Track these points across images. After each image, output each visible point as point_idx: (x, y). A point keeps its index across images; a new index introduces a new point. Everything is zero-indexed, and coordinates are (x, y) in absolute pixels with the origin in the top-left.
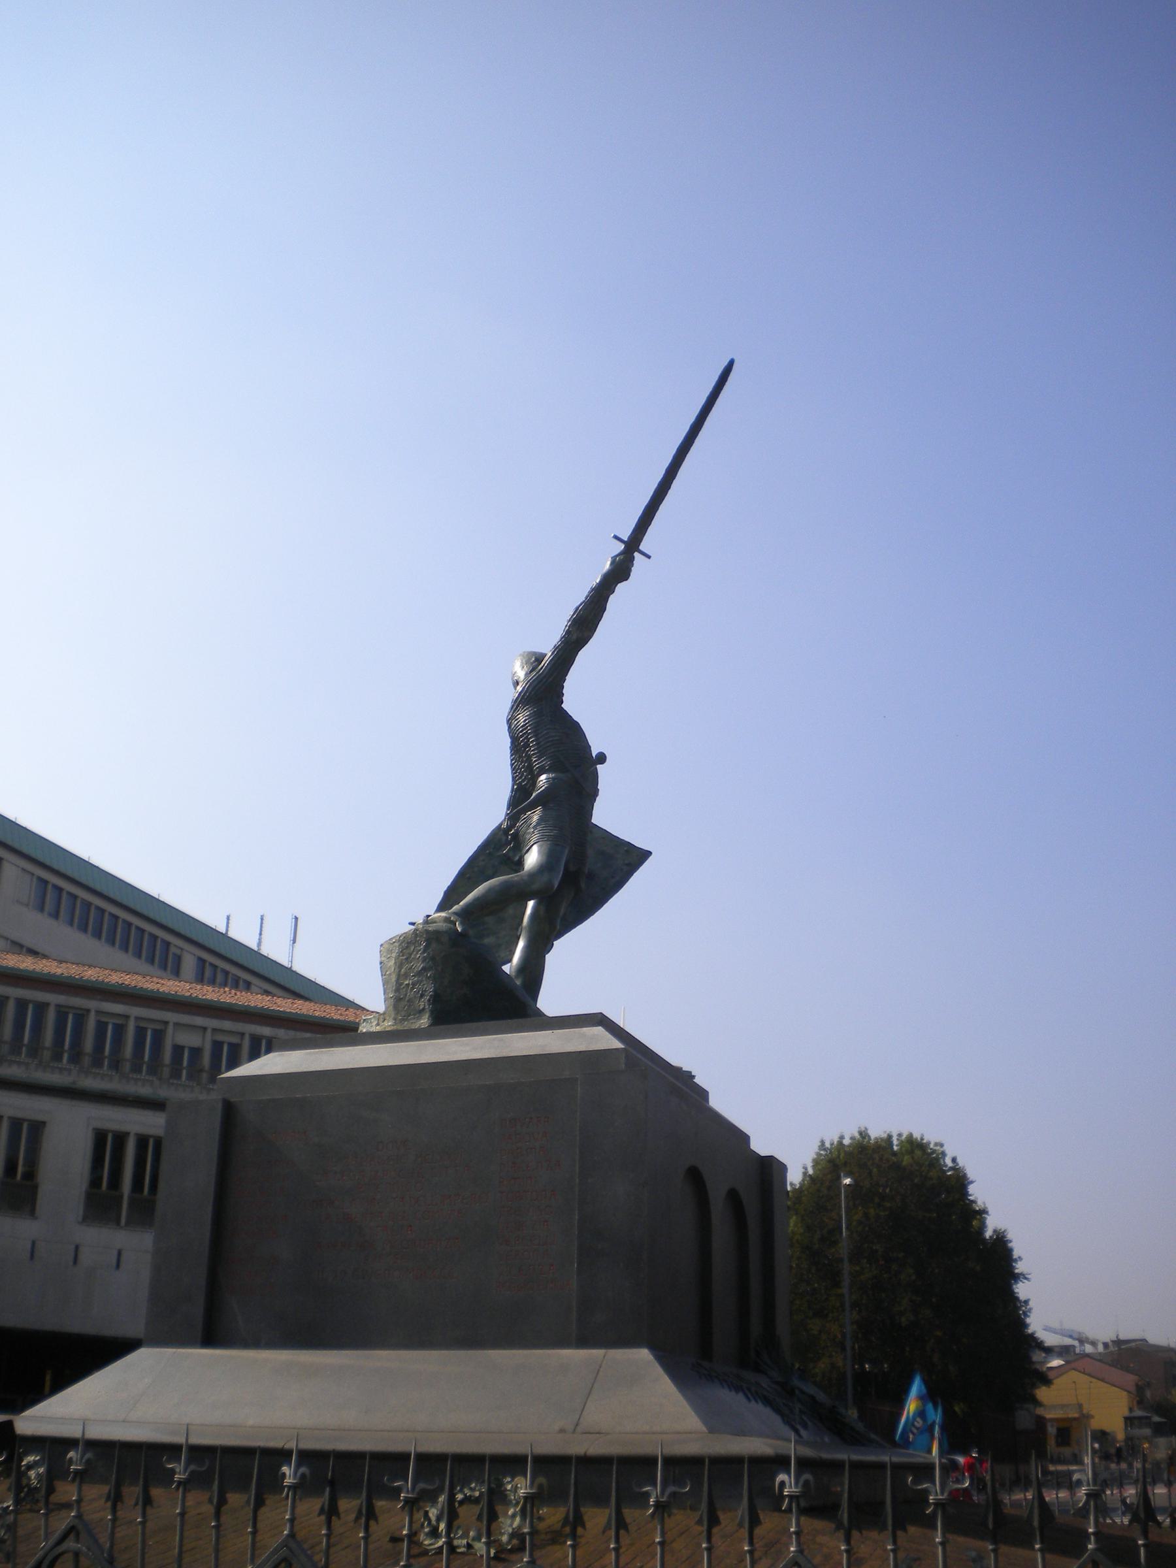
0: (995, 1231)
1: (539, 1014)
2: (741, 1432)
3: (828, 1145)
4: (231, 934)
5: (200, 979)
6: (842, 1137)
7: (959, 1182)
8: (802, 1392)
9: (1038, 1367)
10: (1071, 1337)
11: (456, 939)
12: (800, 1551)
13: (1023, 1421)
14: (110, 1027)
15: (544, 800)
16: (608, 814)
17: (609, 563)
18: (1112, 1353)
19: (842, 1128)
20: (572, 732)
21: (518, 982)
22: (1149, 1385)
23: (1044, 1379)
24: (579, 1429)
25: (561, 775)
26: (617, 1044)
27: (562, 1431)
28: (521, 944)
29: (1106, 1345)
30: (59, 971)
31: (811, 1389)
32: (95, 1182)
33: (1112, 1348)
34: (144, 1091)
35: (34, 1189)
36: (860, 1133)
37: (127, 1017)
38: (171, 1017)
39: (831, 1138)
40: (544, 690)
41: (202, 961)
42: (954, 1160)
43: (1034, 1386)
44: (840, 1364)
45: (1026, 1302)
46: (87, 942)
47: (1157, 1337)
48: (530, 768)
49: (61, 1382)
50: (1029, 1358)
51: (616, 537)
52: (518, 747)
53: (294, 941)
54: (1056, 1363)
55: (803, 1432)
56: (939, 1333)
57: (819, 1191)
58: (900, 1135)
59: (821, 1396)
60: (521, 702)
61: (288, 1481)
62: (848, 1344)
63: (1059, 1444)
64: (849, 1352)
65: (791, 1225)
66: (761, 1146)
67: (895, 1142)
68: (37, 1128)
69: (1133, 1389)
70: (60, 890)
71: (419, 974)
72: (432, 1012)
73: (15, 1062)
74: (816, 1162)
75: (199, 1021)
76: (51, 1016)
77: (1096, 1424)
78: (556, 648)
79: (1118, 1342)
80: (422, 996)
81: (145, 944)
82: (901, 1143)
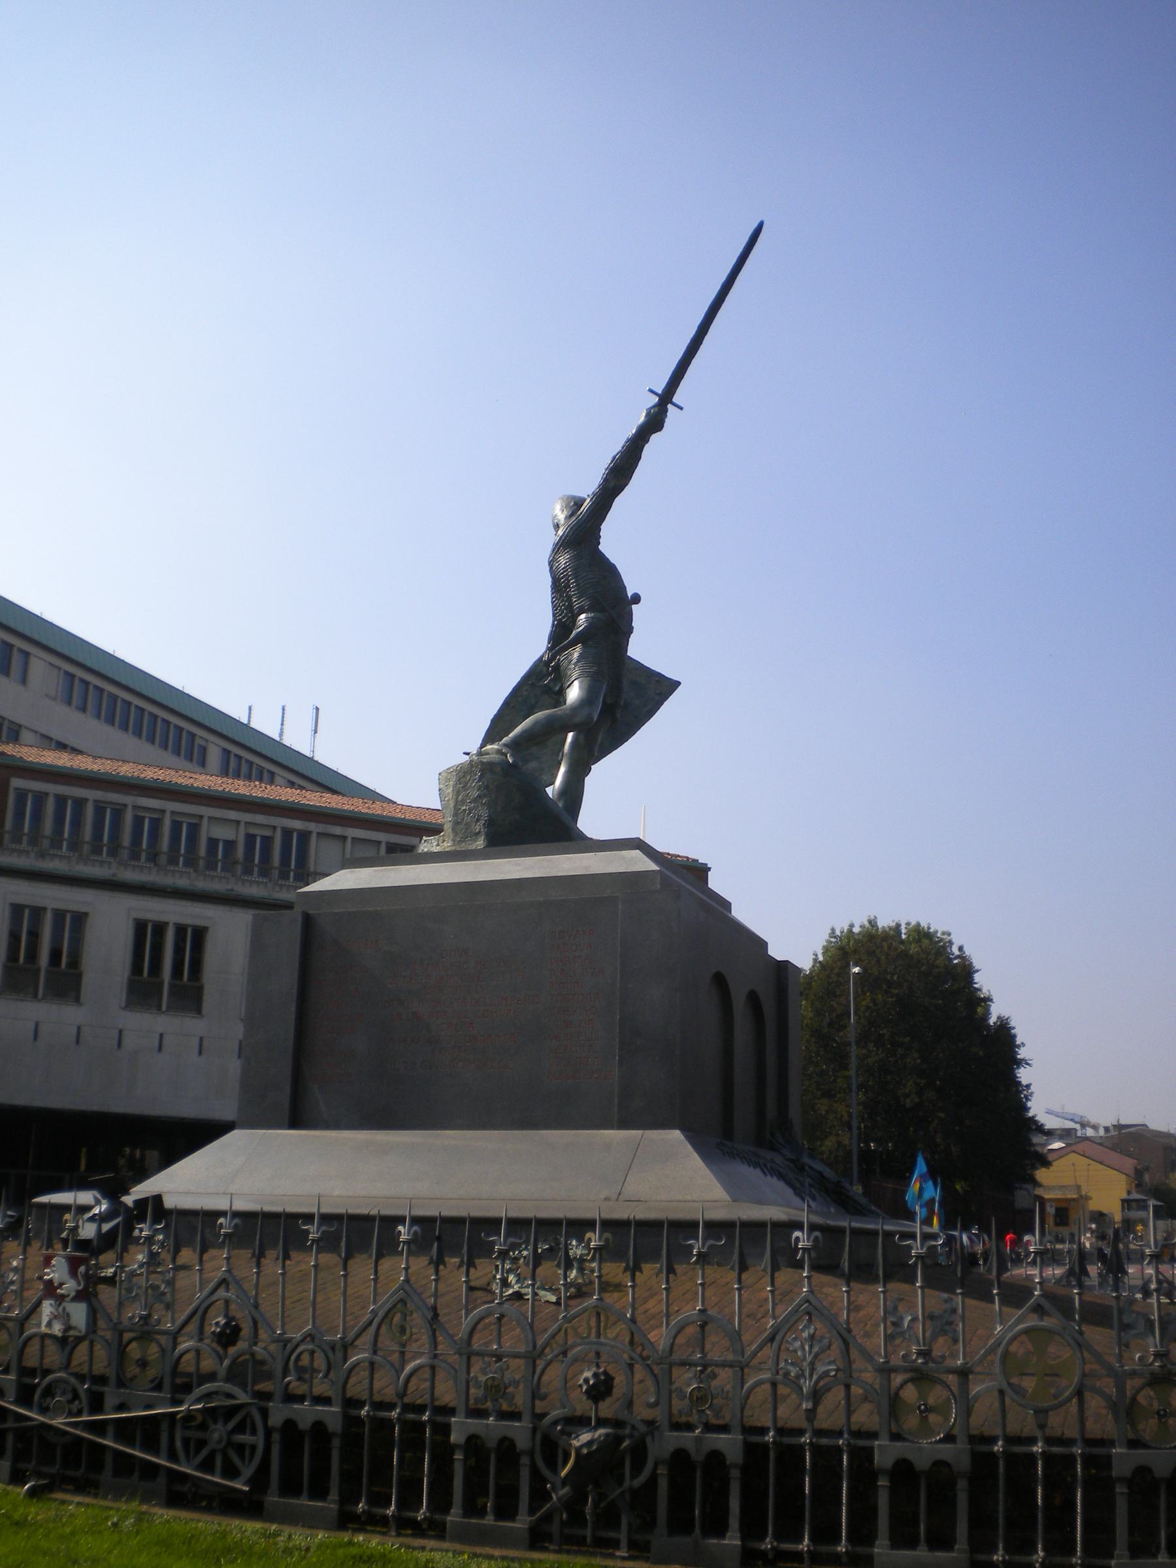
0: (999, 1018)
1: (582, 837)
2: (761, 1202)
3: (838, 933)
4: (253, 725)
5: (225, 772)
6: (852, 926)
7: (966, 971)
8: (810, 1167)
9: (1039, 1149)
10: (1072, 1120)
11: (510, 770)
12: (811, 1291)
13: (1021, 1199)
14: (147, 821)
15: (582, 638)
16: (640, 649)
17: (644, 414)
18: (1112, 1137)
19: (852, 915)
20: (609, 572)
21: (560, 804)
22: (1147, 1169)
23: (1044, 1161)
24: (621, 1198)
25: (598, 615)
26: (653, 867)
27: (606, 1199)
28: (562, 770)
29: (1107, 1129)
30: (95, 768)
31: (820, 1167)
32: (137, 968)
33: (1113, 1133)
34: (182, 882)
35: (79, 976)
36: (870, 922)
37: (163, 811)
38: (206, 811)
39: (841, 926)
40: (582, 534)
41: (227, 752)
42: (961, 949)
43: (1034, 1168)
44: (846, 1142)
45: (1028, 1086)
46: (114, 734)
47: (1158, 1123)
48: (570, 607)
49: (170, 1158)
50: (1029, 1140)
51: (651, 391)
52: (559, 587)
53: (316, 732)
54: (1057, 1145)
55: (812, 1204)
56: (942, 1115)
57: (829, 977)
58: (908, 924)
59: (828, 1172)
60: (563, 545)
61: (403, 1238)
62: (855, 1124)
63: (1057, 1224)
64: (855, 1132)
65: (802, 1010)
66: (777, 952)
67: (904, 931)
68: (80, 919)
69: (1132, 1173)
70: (87, 683)
71: (475, 800)
72: (487, 835)
73: (57, 855)
74: (826, 950)
75: (233, 815)
76: (89, 811)
77: (1093, 1206)
78: (594, 494)
79: (1119, 1127)
80: (478, 820)
81: (184, 742)
82: (908, 934)
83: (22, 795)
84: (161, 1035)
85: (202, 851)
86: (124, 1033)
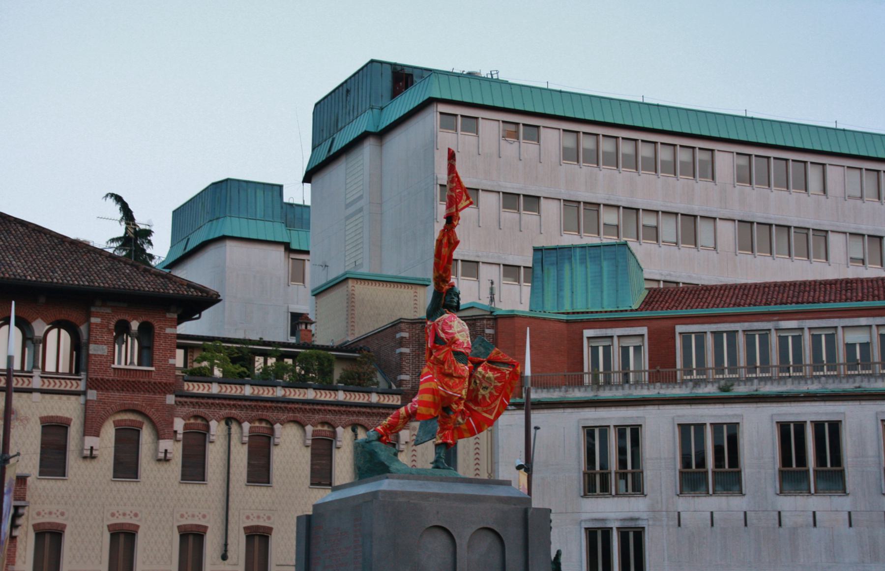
14: (790, 339)
16: (483, 74)
32: (786, 460)
37: (802, 329)
68: (835, 427)
75: (863, 321)
83: (686, 336)
84: (814, 513)
85: (841, 357)
86: (782, 514)
